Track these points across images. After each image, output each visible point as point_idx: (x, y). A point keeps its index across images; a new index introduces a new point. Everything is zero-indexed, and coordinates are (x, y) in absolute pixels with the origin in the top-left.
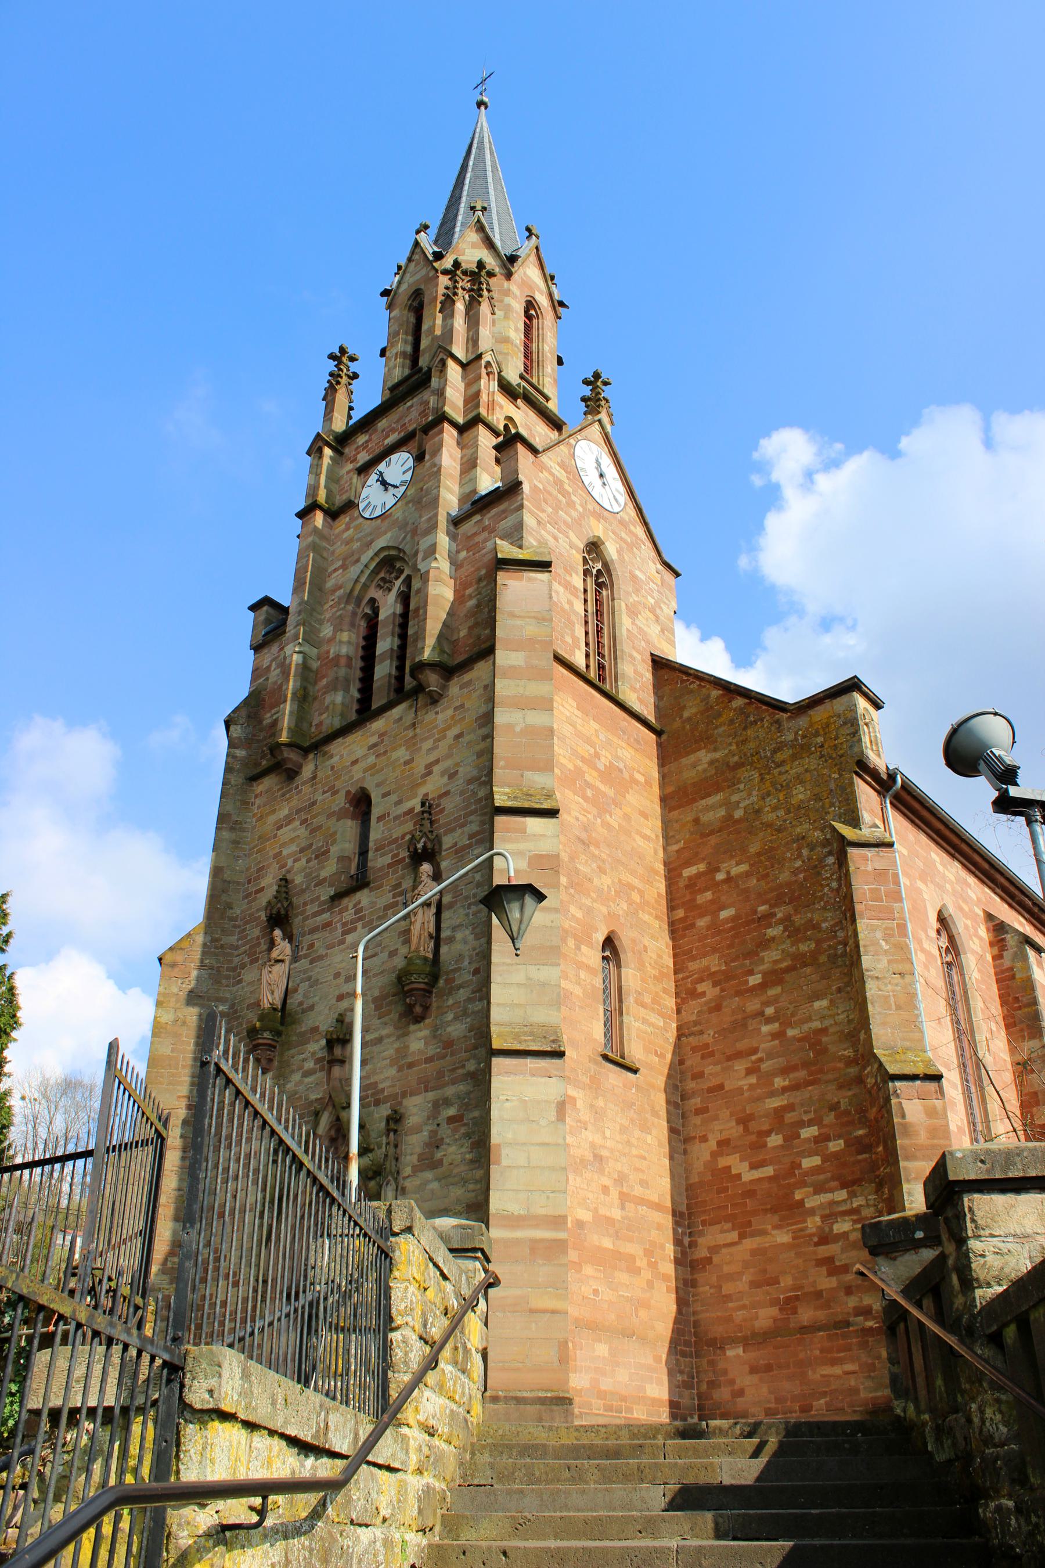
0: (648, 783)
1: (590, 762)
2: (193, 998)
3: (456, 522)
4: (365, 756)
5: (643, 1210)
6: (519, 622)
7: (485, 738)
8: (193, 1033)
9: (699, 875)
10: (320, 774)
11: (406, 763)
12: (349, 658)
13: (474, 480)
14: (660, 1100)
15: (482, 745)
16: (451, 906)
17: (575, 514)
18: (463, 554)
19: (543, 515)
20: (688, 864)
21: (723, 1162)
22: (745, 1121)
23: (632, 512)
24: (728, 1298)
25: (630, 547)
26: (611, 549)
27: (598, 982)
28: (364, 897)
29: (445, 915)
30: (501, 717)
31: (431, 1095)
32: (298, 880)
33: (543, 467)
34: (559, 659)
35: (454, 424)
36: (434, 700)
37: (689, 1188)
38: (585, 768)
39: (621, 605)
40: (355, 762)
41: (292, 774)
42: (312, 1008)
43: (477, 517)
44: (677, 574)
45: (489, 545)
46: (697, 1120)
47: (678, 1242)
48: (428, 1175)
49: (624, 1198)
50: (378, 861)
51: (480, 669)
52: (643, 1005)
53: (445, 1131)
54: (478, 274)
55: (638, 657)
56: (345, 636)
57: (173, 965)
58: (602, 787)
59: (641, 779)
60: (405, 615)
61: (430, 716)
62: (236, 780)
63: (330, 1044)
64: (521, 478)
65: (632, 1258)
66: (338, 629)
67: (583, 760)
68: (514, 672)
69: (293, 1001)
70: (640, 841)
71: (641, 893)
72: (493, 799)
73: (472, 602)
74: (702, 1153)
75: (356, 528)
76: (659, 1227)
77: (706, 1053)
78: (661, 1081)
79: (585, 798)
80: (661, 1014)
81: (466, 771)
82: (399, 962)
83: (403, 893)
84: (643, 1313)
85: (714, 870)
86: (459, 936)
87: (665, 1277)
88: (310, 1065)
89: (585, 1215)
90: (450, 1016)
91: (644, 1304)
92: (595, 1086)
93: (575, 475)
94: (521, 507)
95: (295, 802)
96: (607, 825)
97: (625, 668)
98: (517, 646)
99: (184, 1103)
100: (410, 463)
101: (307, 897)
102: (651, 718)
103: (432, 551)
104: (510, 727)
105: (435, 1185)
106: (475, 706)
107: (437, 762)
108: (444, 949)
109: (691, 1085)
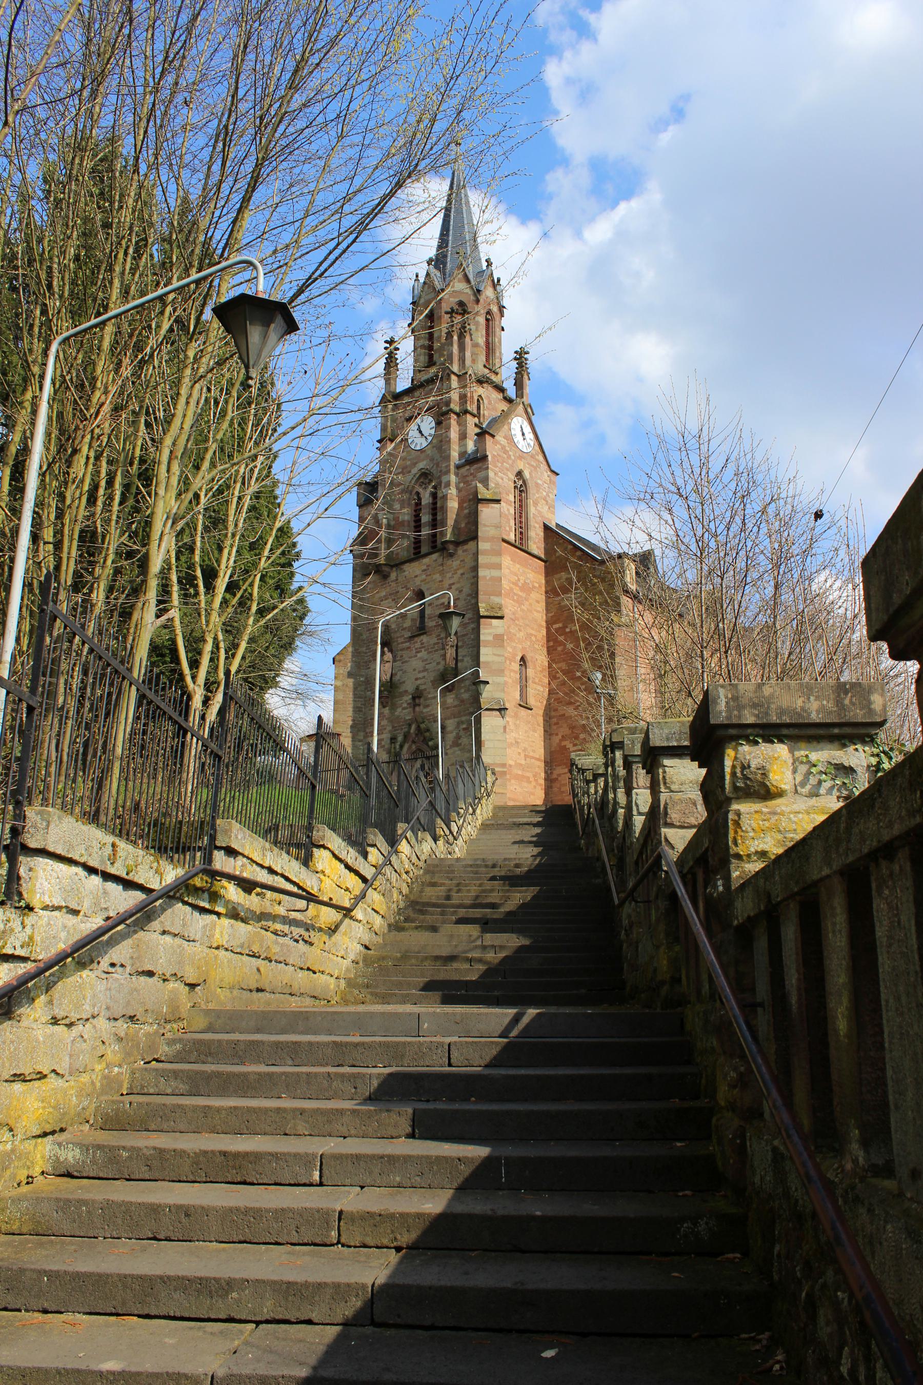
0: (540, 586)
1: (516, 584)
2: (350, 675)
3: (458, 467)
4: (421, 575)
5: (533, 761)
6: (488, 529)
7: (474, 577)
8: (352, 689)
9: (560, 628)
10: (400, 579)
11: (440, 581)
12: (409, 522)
13: (465, 445)
14: (541, 720)
15: (473, 580)
16: (462, 647)
17: (510, 462)
18: (462, 485)
19: (497, 469)
20: (555, 623)
21: (563, 743)
22: (572, 728)
23: (537, 448)
24: (563, 792)
25: (535, 468)
26: (527, 474)
27: (518, 676)
28: (424, 638)
29: (459, 650)
30: (482, 573)
31: (456, 720)
32: (393, 626)
33: (498, 443)
34: (504, 541)
35: (456, 413)
36: (451, 555)
37: (551, 752)
38: (514, 587)
39: (530, 502)
40: (416, 576)
41: (385, 577)
42: (404, 682)
43: (467, 467)
44: (557, 474)
45: (473, 483)
46: (555, 727)
47: (546, 772)
48: (456, 749)
49: (526, 757)
50: (430, 624)
51: (471, 544)
52: (535, 683)
53: (462, 733)
54: (462, 308)
55: (537, 526)
56: (405, 510)
57: (340, 661)
58: (521, 594)
59: (537, 585)
60: (435, 503)
61: (450, 562)
62: (358, 575)
63: (414, 698)
64: (488, 453)
65: (528, 778)
66: (402, 507)
67: (513, 583)
68: (486, 552)
69: (396, 678)
70: (536, 614)
71: (535, 636)
72: (479, 611)
73: (466, 511)
74: (556, 740)
75: (408, 452)
76: (539, 767)
77: (558, 700)
78: (541, 712)
79: (514, 600)
80: (542, 686)
81: (467, 590)
82: (441, 667)
83: (441, 639)
84: (532, 797)
85: (565, 627)
86: (465, 659)
87: (541, 785)
88: (405, 705)
89: (511, 762)
90: (463, 691)
91: (533, 794)
92: (516, 716)
93: (510, 439)
94: (487, 468)
95: (388, 589)
96: (522, 610)
97: (532, 534)
98: (488, 540)
99: (351, 719)
100: (433, 424)
101: (398, 635)
102: (543, 556)
103: (448, 484)
104: (485, 577)
105: (459, 752)
106: (469, 563)
107: (453, 584)
108: (459, 664)
109: (553, 714)
